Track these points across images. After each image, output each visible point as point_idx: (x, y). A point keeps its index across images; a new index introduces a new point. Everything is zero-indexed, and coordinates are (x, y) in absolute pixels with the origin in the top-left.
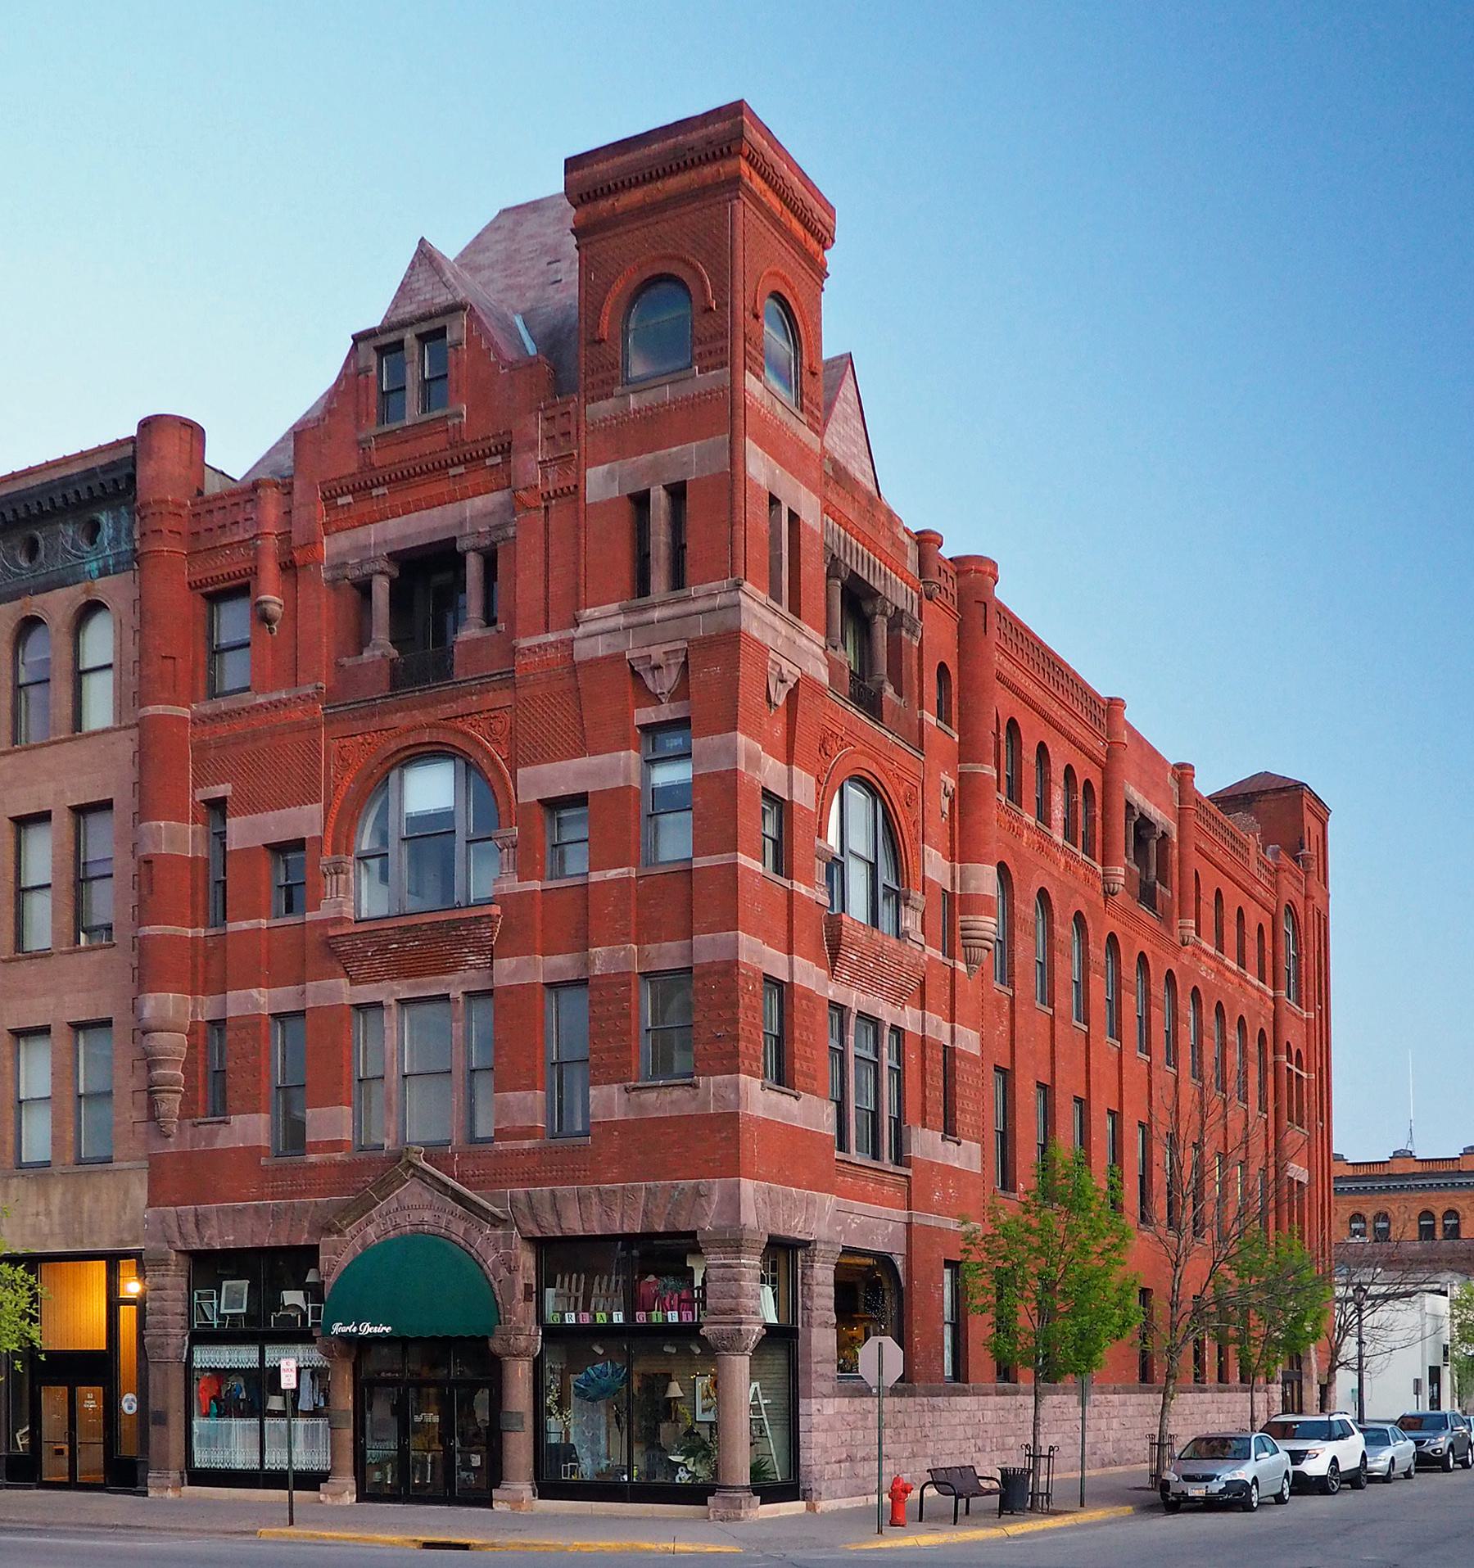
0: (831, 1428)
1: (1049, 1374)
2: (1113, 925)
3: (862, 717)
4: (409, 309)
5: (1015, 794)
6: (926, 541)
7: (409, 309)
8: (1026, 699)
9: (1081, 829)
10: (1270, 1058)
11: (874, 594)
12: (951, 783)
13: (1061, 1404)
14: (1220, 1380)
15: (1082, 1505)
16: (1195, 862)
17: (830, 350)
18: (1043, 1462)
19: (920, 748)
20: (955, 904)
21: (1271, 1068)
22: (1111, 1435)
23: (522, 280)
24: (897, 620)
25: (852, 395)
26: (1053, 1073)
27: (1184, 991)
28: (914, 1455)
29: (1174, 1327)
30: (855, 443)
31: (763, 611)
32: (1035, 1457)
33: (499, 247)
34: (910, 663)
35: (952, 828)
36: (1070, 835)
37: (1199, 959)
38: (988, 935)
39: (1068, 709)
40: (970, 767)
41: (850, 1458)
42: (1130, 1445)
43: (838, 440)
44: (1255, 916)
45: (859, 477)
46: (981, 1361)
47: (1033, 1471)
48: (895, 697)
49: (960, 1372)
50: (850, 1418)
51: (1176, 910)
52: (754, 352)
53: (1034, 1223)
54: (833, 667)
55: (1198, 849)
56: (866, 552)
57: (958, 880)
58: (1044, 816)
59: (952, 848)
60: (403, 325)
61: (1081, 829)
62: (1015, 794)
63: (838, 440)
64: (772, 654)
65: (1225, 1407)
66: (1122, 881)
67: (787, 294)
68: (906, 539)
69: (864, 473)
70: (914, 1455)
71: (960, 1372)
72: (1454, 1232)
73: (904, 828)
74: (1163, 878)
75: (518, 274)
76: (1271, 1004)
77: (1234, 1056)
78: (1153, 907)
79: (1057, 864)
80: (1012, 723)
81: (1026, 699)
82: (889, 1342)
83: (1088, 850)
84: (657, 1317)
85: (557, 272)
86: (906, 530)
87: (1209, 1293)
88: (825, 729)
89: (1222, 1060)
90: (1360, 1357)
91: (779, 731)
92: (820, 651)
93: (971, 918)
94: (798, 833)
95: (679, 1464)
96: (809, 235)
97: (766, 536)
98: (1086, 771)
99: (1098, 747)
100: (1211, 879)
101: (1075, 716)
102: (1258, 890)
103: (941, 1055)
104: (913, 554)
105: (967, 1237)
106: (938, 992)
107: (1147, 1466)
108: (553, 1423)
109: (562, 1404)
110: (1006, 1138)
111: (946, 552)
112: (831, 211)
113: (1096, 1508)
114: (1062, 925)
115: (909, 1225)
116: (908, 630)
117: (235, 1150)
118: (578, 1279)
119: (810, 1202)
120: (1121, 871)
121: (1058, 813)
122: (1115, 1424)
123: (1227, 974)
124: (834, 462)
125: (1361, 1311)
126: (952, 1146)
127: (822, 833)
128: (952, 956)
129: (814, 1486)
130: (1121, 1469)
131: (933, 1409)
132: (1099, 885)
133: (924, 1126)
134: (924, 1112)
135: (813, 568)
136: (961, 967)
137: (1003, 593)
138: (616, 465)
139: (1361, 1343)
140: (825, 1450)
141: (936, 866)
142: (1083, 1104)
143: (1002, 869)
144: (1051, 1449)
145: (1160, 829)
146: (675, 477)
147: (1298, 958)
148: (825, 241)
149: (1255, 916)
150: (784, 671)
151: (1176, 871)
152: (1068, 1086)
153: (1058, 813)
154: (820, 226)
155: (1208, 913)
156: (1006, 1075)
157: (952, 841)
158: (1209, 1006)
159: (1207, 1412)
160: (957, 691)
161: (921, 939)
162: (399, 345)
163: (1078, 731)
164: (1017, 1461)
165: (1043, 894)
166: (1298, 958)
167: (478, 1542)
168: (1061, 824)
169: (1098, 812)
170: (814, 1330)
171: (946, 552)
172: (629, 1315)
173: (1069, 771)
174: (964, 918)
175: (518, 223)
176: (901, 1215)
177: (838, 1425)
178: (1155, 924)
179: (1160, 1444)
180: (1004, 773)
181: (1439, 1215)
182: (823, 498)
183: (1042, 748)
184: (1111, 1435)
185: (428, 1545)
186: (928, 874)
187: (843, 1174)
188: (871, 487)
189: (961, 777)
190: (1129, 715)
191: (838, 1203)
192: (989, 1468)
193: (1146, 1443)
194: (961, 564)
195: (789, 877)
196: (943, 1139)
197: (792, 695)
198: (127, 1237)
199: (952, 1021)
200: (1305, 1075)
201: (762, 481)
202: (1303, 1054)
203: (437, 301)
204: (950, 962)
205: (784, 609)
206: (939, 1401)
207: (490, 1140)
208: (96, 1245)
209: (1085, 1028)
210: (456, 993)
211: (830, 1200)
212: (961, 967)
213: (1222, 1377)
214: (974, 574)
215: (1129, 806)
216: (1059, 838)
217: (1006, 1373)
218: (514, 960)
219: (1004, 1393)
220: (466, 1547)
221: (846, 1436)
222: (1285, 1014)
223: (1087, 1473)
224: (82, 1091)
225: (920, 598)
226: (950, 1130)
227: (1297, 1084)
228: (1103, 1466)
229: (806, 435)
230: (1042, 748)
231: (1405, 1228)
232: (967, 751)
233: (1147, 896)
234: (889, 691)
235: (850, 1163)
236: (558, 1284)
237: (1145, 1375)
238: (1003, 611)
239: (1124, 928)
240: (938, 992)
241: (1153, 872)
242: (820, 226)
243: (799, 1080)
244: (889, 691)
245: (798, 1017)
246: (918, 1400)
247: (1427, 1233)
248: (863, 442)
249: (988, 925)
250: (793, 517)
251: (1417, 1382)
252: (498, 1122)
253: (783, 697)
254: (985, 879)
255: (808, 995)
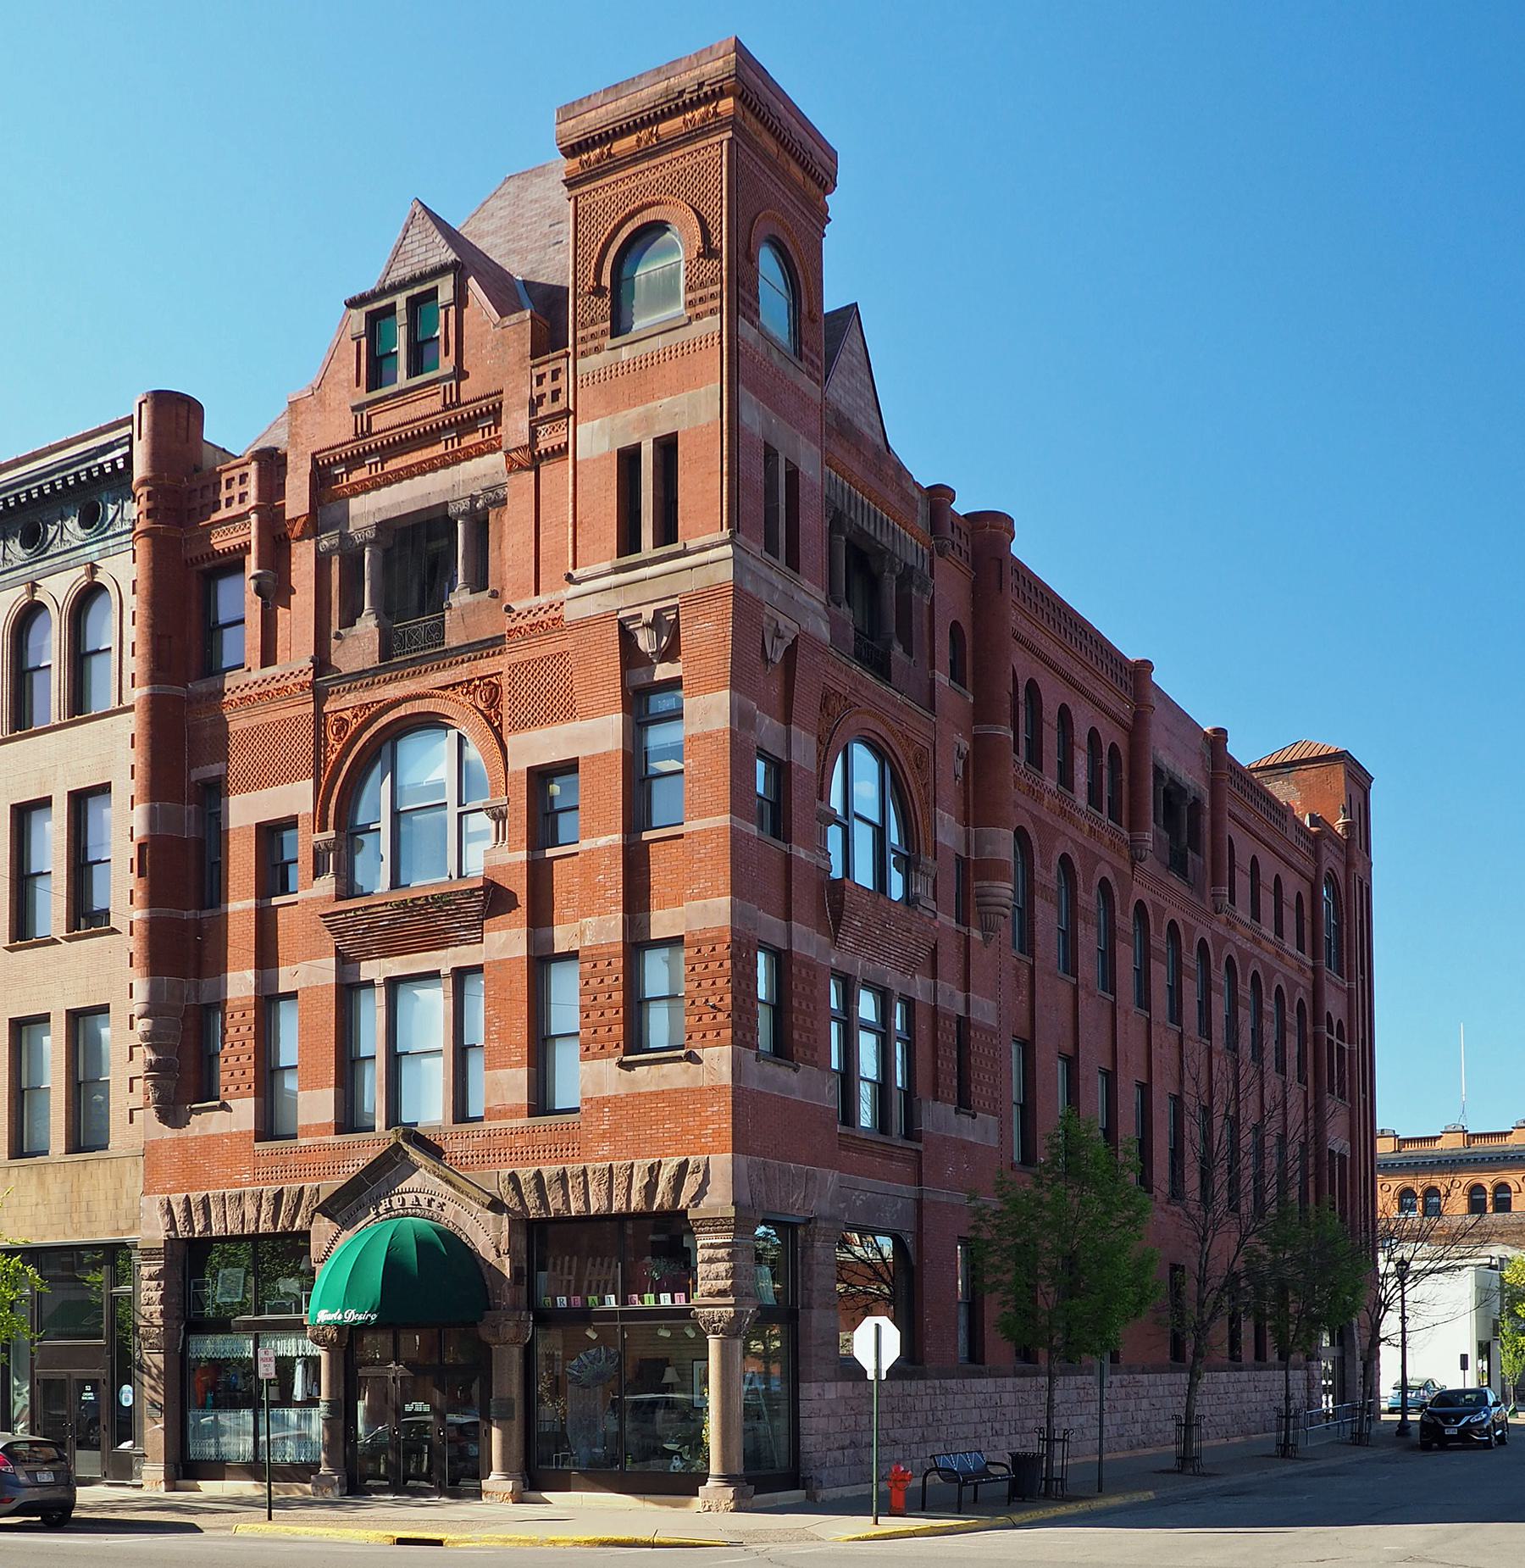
0: (834, 1414)
1: (1070, 1358)
2: (1140, 892)
3: (868, 676)
4: (401, 272)
5: (1035, 757)
6: (940, 495)
7: (402, 272)
8: (1046, 660)
9: (1106, 794)
10: (1309, 1030)
11: (882, 553)
12: (965, 745)
13: (1068, 1387)
14: (1232, 1358)
15: (1100, 1490)
16: (1230, 829)
17: (832, 302)
18: (1058, 1446)
19: (932, 708)
20: (971, 869)
21: (1310, 1039)
22: (1141, 1416)
23: (523, 243)
24: (907, 577)
25: (857, 347)
26: (1076, 1044)
27: (1218, 962)
28: (924, 1440)
29: (1201, 1303)
30: (861, 395)
31: (758, 565)
32: (1050, 1441)
33: (502, 213)
34: (919, 621)
35: (966, 791)
36: (1094, 798)
37: (1234, 928)
38: (1005, 901)
39: (1091, 671)
40: (986, 729)
41: (853, 1444)
42: (1160, 1426)
43: (840, 391)
44: (1293, 885)
45: (866, 430)
46: (998, 1347)
47: (1050, 1455)
48: (904, 658)
49: (976, 1354)
50: (854, 1403)
51: (1209, 879)
52: (747, 297)
53: (1048, 1197)
54: (834, 623)
55: (1233, 816)
56: (872, 506)
57: (973, 845)
58: (1066, 779)
59: (966, 813)
60: (396, 288)
61: (1106, 794)
62: (1035, 757)
63: (840, 391)
64: (767, 609)
65: (1261, 1386)
66: (1150, 846)
67: (783, 236)
68: (916, 494)
69: (871, 427)
70: (924, 1440)
71: (976, 1354)
72: (1503, 1205)
73: (914, 792)
74: (1195, 843)
75: (520, 238)
76: (1309, 974)
77: (1270, 1028)
78: (1183, 873)
79: (1079, 829)
80: (1032, 686)
81: (1046, 660)
82: (885, 1322)
83: (1114, 815)
84: (649, 1300)
85: (559, 233)
86: (916, 484)
87: (1240, 1266)
88: (825, 687)
89: (1257, 1033)
90: (1404, 1331)
91: (776, 690)
92: (821, 607)
93: (986, 883)
94: (797, 795)
95: (674, 1453)
96: (808, 180)
97: (761, 487)
98: (1111, 735)
99: (1125, 710)
100: (1245, 849)
101: (1098, 677)
102: (1295, 859)
103: (954, 1026)
104: (923, 509)
105: (977, 1212)
106: (949, 963)
107: (1173, 1448)
108: (547, 1411)
109: (557, 1389)
110: (1027, 1110)
111: (961, 507)
112: (832, 155)
113: (1115, 1494)
114: (1088, 891)
115: (919, 1202)
116: (918, 588)
117: (230, 1136)
118: (570, 1261)
119: (809, 1177)
120: (1149, 836)
121: (1081, 778)
122: (1145, 1404)
123: (1264, 942)
124: (838, 414)
125: (1403, 1285)
126: (966, 1119)
127: (823, 793)
128: (966, 924)
129: (814, 1473)
130: (1150, 1451)
131: (946, 1392)
132: (1126, 852)
133: (936, 1099)
134: (935, 1084)
135: (812, 522)
136: (976, 934)
137: (1018, 549)
138: (606, 419)
139: (1403, 1318)
140: (826, 1436)
141: (949, 831)
142: (1110, 1077)
143: (1021, 835)
144: (1066, 1432)
145: (1191, 794)
146: (664, 429)
147: (1339, 928)
148: (827, 183)
149: (1293, 885)
150: (781, 627)
151: (1208, 837)
152: (1093, 1059)
153: (1081, 778)
154: (819, 169)
155: (1243, 882)
156: (1028, 1047)
157: (966, 804)
158: (1244, 976)
159: (1243, 1391)
160: (975, 655)
161: (932, 905)
162: (391, 310)
163: (1102, 693)
164: (1034, 1447)
165: (1065, 860)
166: (1339, 928)
167: (451, 1537)
168: (1085, 788)
169: (1125, 776)
170: (815, 1313)
171: (961, 507)
172: (624, 1301)
173: (1093, 735)
174: (979, 884)
175: (524, 189)
176: (909, 1191)
177: (841, 1410)
178: (1185, 892)
179: (1188, 1425)
180: (1022, 735)
181: (1489, 1188)
182: (825, 450)
183: (1064, 713)
184: (1141, 1416)
185: (401, 1541)
186: (940, 838)
187: (847, 1149)
188: (880, 441)
189: (976, 740)
190: (1156, 677)
191: (841, 1180)
192: (1000, 1453)
193: (1171, 1426)
194: (977, 519)
195: (788, 840)
196: (957, 1112)
197: (791, 652)
198: (123, 1226)
199: (966, 989)
200: (1346, 1046)
201: (757, 430)
202: (1345, 1024)
203: (430, 261)
204: (964, 930)
205: (781, 562)
206: (952, 1383)
207: (480, 1119)
208: (92, 1233)
209: (1111, 997)
210: (446, 970)
211: (832, 1177)
212: (976, 934)
213: (1260, 1354)
214: (991, 530)
215: (1158, 772)
216: (1082, 801)
217: (1026, 1355)
218: (504, 933)
219: (1023, 1374)
220: (439, 1543)
221: (850, 1422)
222: (1326, 984)
223: (1106, 1457)
224: (81, 1078)
225: (931, 554)
226: (964, 1103)
227: (1340, 1060)
228: (1132, 1448)
229: (806, 383)
230: (1064, 713)
231: (1457, 1205)
232: (981, 712)
233: (1178, 864)
234: (898, 650)
235: (854, 1138)
236: (550, 1267)
237: (1177, 1353)
238: (1020, 569)
239: (1153, 896)
240: (949, 963)
241: (1185, 839)
242: (819, 169)
243: (798, 1051)
244: (898, 650)
245: (797, 986)
246: (929, 1383)
247: (1476, 1206)
248: (870, 395)
249: (1005, 890)
250: (793, 475)
251: (1464, 1358)
252: (487, 1100)
253: (781, 654)
254: (1003, 845)
255: (809, 964)
